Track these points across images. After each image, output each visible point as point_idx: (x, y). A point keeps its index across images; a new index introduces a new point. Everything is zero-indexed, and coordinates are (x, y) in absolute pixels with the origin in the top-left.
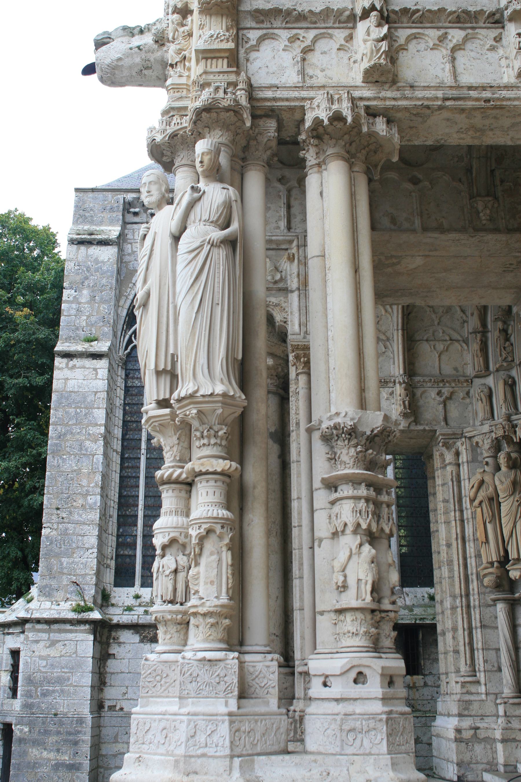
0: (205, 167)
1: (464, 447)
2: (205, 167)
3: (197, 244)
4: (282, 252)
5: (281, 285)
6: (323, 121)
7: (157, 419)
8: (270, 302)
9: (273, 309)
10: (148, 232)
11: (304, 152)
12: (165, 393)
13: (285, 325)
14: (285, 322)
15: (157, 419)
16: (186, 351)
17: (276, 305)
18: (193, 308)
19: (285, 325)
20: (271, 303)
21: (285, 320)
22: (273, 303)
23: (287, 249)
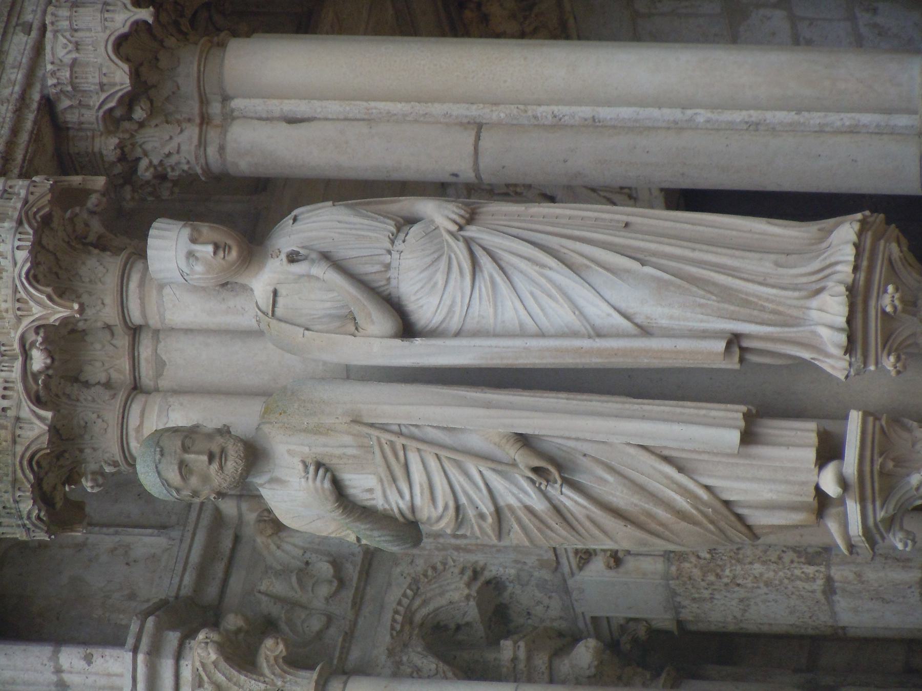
0: (229, 242)
1: (851, 576)
2: (229, 242)
3: (460, 249)
4: (244, 553)
5: (352, 572)
6: (138, 26)
7: (868, 454)
8: (399, 603)
9: (425, 603)
10: (327, 470)
11: (144, 163)
12: (808, 430)
13: (482, 579)
14: (476, 574)
15: (868, 454)
16: (733, 304)
17: (415, 585)
18: (628, 271)
19: (482, 579)
20: (405, 602)
21: (469, 573)
22: (405, 595)
23: (237, 539)
